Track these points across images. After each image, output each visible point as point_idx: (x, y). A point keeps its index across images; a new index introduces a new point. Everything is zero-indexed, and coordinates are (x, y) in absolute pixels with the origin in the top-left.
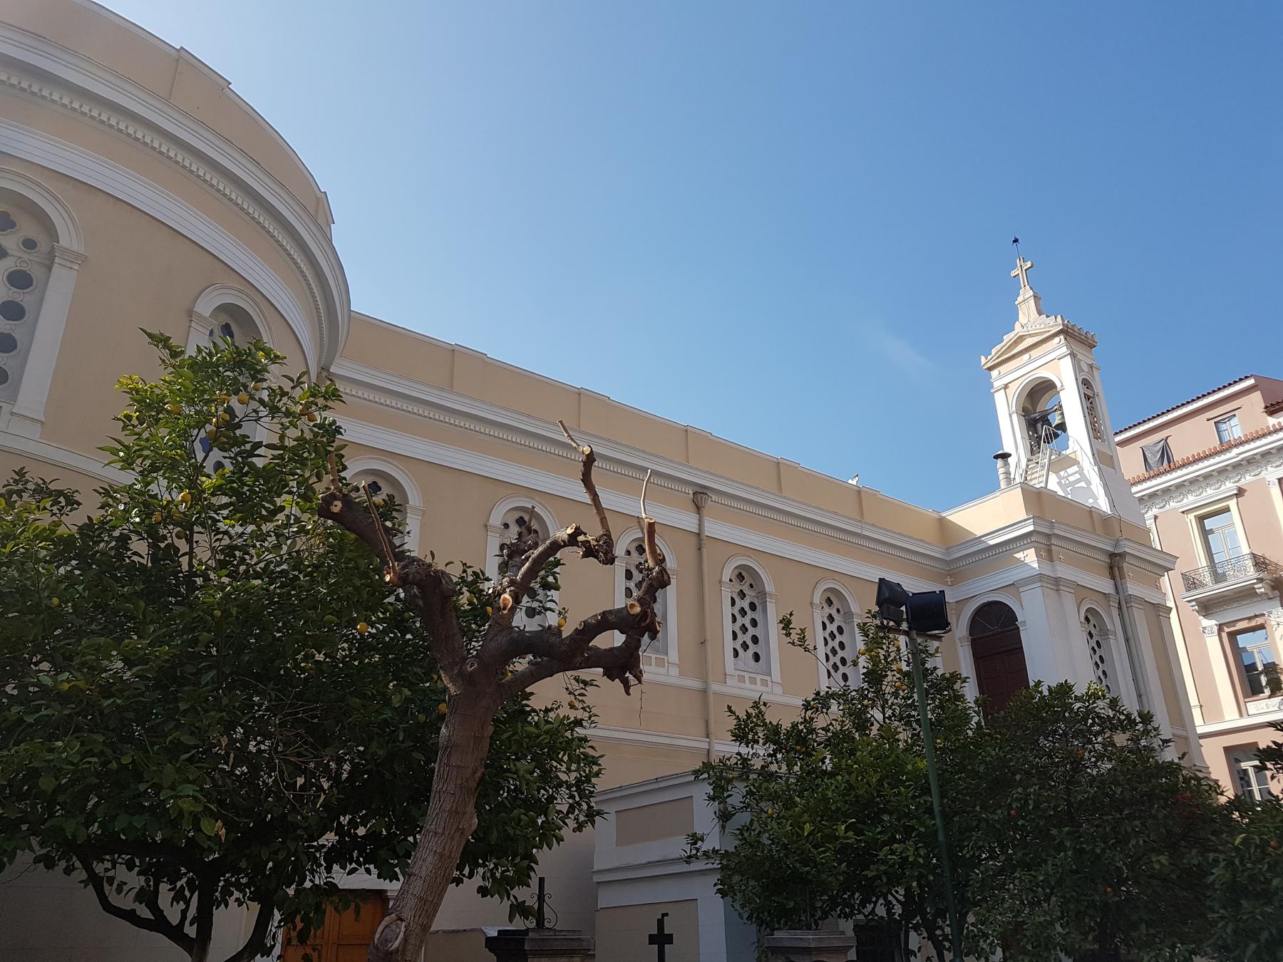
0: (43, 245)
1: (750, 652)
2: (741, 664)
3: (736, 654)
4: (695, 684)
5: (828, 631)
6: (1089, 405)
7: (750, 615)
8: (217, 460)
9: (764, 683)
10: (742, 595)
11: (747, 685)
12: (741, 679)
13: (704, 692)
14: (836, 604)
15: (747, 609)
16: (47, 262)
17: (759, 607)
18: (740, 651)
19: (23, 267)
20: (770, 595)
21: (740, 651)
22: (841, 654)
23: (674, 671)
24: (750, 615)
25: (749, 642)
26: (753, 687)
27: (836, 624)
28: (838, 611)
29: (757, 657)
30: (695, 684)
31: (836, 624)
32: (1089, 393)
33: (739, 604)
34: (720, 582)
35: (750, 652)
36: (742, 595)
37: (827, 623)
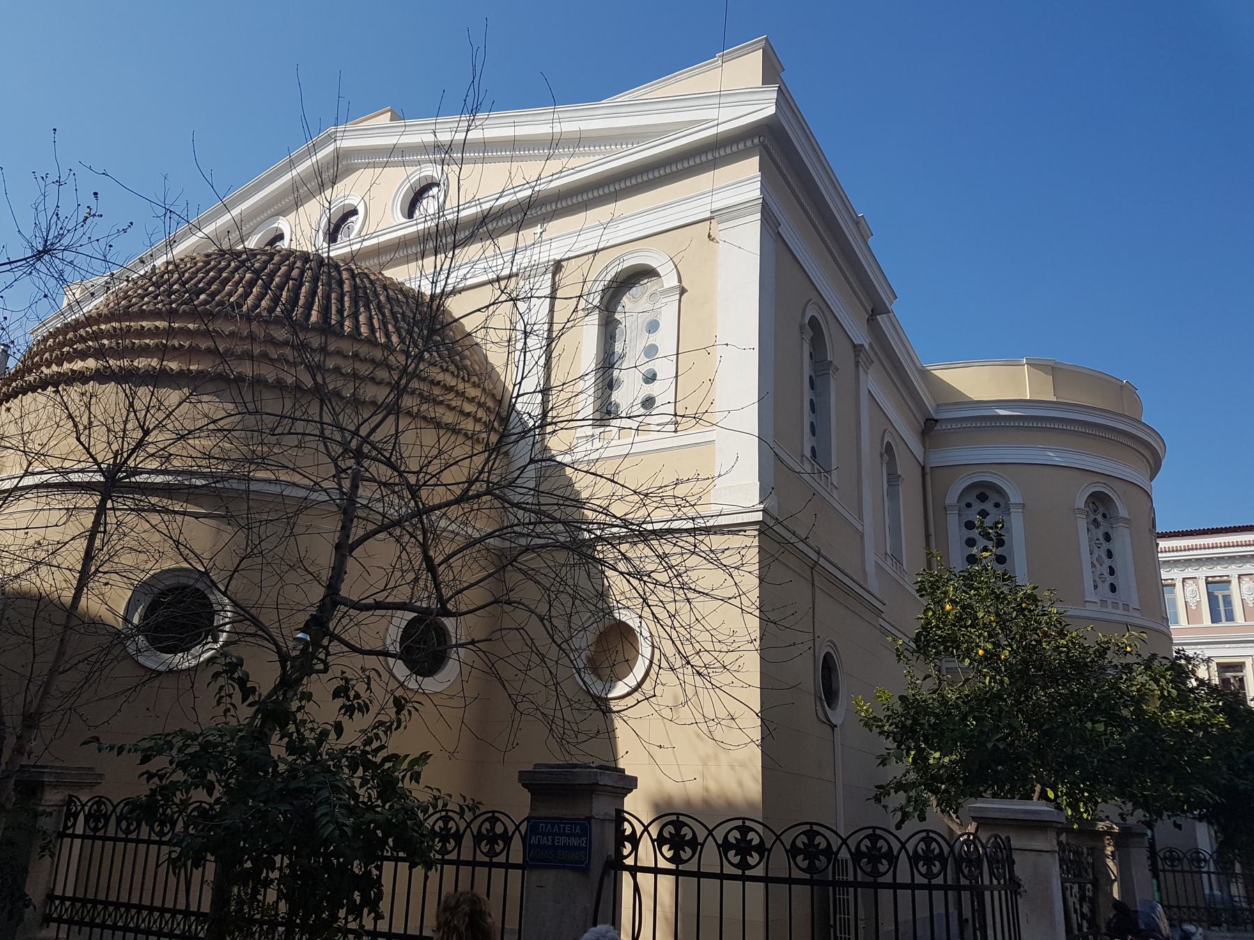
11: (1110, 609)
26: (1114, 611)
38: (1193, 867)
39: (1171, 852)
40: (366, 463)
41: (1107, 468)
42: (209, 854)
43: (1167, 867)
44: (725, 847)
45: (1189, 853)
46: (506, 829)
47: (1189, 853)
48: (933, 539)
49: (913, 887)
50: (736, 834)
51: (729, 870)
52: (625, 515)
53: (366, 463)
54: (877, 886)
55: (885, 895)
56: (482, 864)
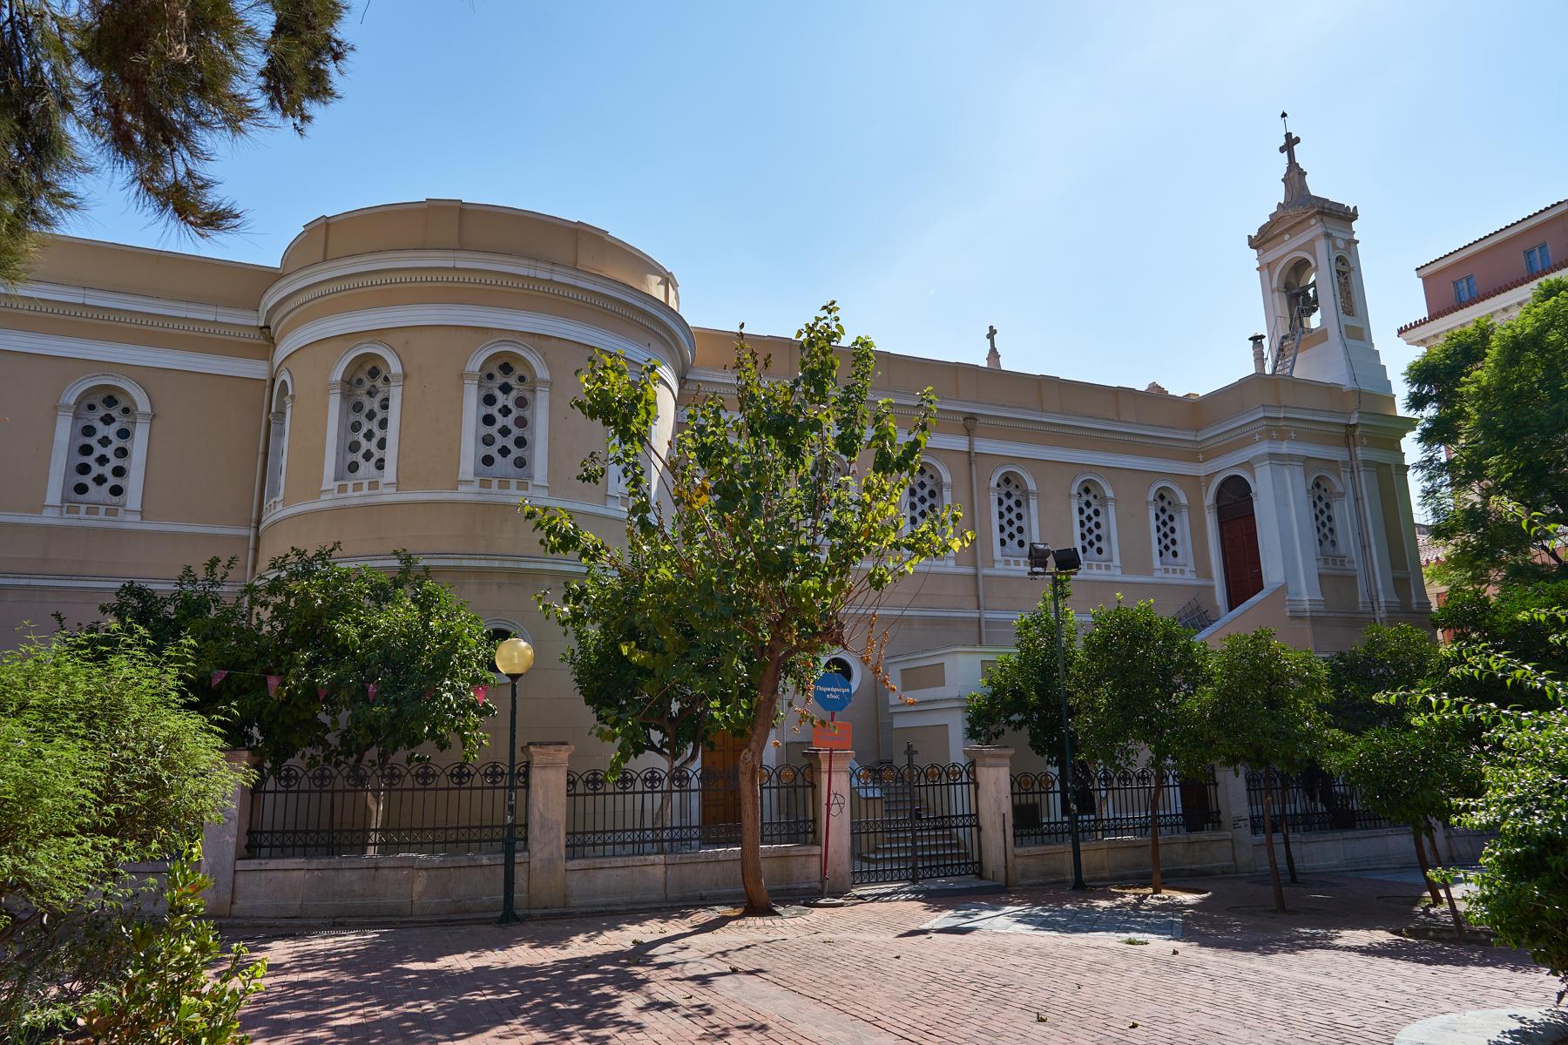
0: (528, 379)
1: (1170, 551)
2: (1007, 550)
3: (1003, 543)
4: (970, 570)
5: (1320, 521)
6: (1342, 280)
7: (1016, 510)
8: (504, 459)
9: (1108, 568)
10: (1009, 495)
11: (1012, 566)
12: (1007, 563)
13: (976, 575)
14: (1093, 491)
15: (1013, 506)
16: (1466, 296)
17: (1024, 503)
18: (1164, 551)
19: (124, 426)
20: (1033, 493)
21: (1164, 551)
22: (1096, 532)
23: (1118, 572)
24: (1016, 510)
25: (1015, 533)
26: (1016, 567)
27: (1092, 509)
28: (1095, 497)
29: (1100, 551)
30: (970, 570)
31: (1092, 509)
32: (1343, 269)
33: (1006, 502)
34: (989, 488)
35: (1170, 551)
36: (1009, 495)
37: (1160, 514)
38: (312, 785)
39: (595, 774)
40: (306, 87)
41: (547, 328)
42: (50, 805)
43: (313, 787)
44: (645, 780)
45: (644, 773)
46: (297, 773)
47: (644, 773)
48: (261, 449)
49: (1119, 789)
50: (491, 769)
51: (588, 791)
52: (603, 351)
53: (306, 87)
54: (1048, 793)
55: (1051, 795)
56: (619, 793)
